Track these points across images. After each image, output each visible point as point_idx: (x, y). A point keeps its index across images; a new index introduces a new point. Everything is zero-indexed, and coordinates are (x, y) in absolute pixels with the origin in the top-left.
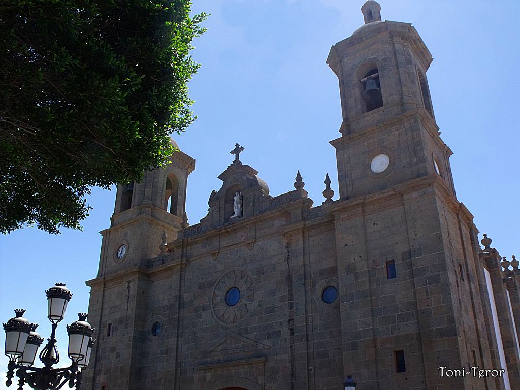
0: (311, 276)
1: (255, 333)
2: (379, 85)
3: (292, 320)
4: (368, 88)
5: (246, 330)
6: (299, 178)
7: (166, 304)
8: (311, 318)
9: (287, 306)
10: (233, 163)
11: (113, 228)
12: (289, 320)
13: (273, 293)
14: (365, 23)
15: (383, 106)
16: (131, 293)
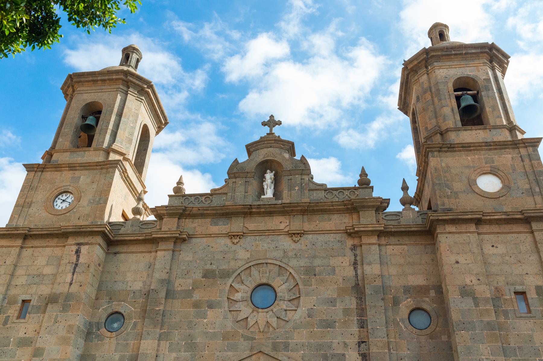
0: (391, 291)
1: (302, 352)
2: (97, 124)
3: (363, 342)
4: (463, 104)
5: (286, 346)
6: (181, 177)
7: (139, 288)
8: (395, 344)
9: (356, 322)
10: (266, 135)
11: (252, 157)
12: (359, 342)
13: (332, 302)
14: (121, 64)
15: (463, 125)
16: (81, 260)
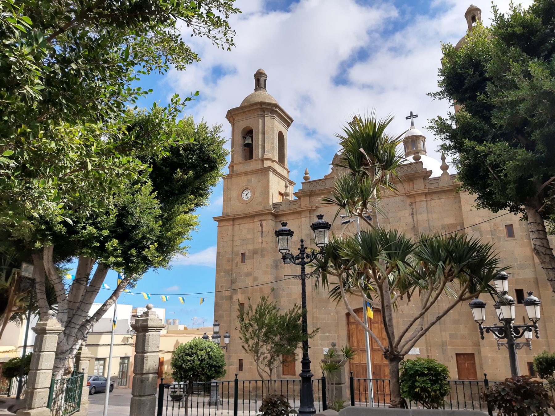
16: (264, 229)
